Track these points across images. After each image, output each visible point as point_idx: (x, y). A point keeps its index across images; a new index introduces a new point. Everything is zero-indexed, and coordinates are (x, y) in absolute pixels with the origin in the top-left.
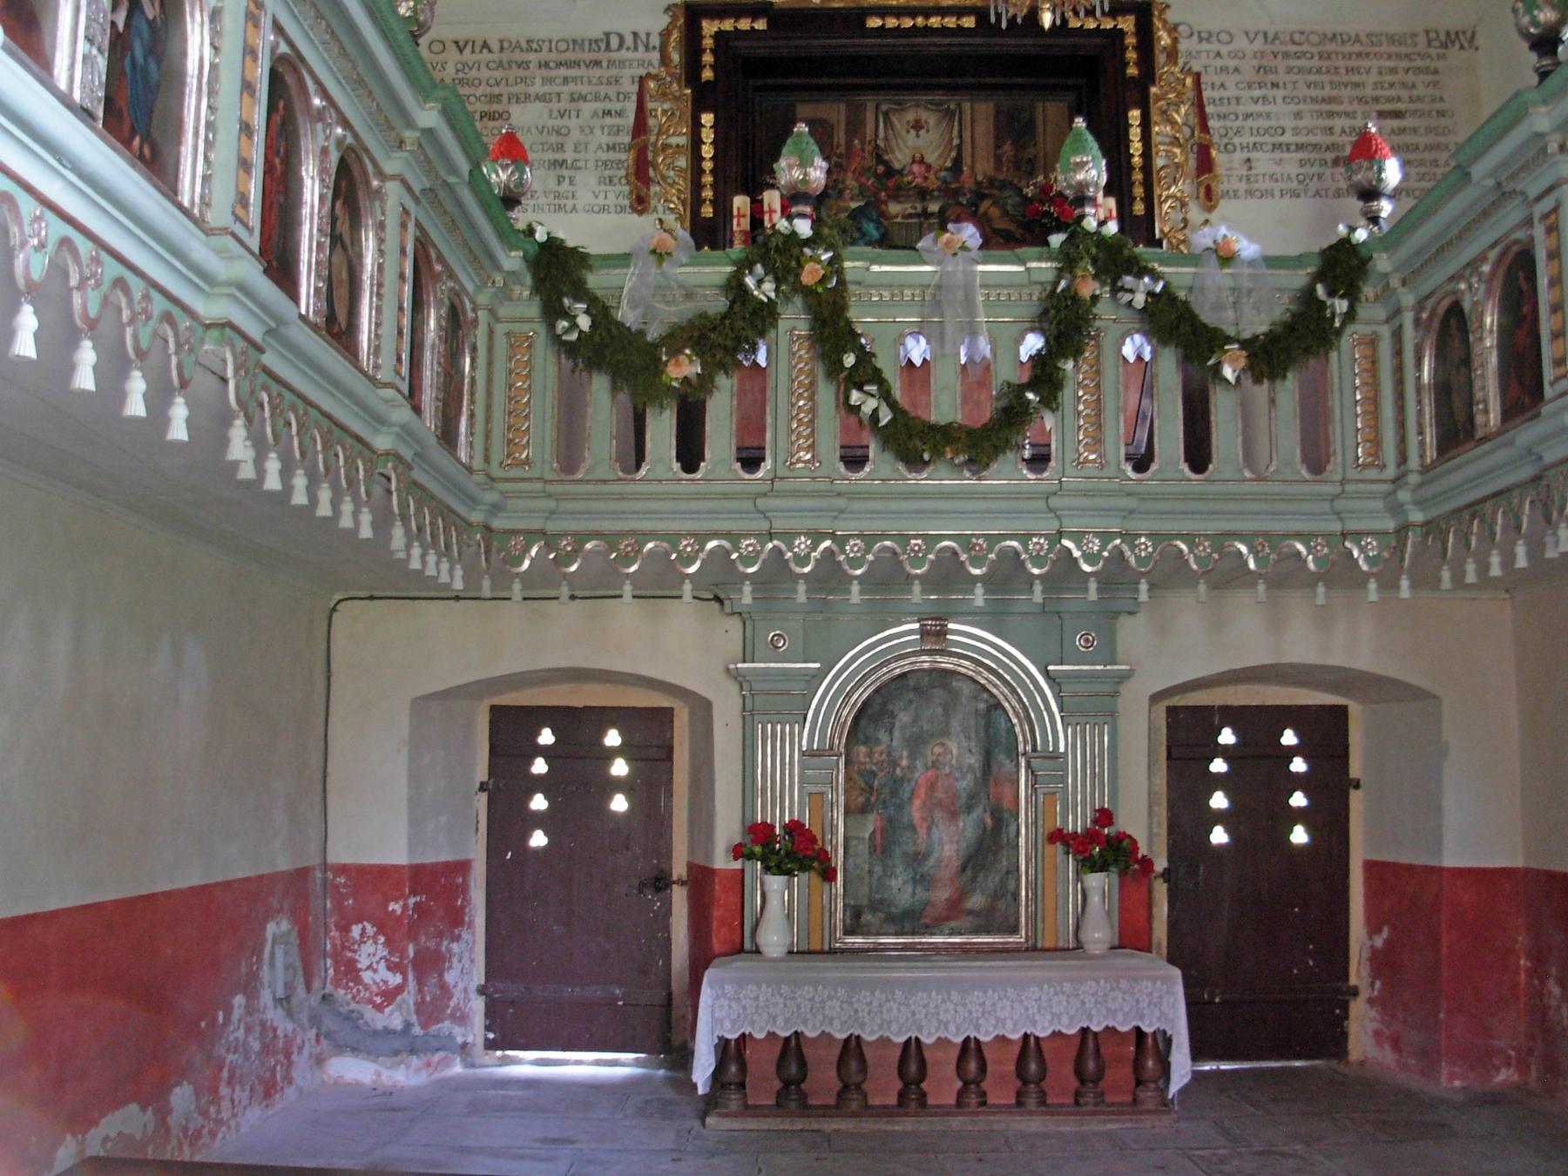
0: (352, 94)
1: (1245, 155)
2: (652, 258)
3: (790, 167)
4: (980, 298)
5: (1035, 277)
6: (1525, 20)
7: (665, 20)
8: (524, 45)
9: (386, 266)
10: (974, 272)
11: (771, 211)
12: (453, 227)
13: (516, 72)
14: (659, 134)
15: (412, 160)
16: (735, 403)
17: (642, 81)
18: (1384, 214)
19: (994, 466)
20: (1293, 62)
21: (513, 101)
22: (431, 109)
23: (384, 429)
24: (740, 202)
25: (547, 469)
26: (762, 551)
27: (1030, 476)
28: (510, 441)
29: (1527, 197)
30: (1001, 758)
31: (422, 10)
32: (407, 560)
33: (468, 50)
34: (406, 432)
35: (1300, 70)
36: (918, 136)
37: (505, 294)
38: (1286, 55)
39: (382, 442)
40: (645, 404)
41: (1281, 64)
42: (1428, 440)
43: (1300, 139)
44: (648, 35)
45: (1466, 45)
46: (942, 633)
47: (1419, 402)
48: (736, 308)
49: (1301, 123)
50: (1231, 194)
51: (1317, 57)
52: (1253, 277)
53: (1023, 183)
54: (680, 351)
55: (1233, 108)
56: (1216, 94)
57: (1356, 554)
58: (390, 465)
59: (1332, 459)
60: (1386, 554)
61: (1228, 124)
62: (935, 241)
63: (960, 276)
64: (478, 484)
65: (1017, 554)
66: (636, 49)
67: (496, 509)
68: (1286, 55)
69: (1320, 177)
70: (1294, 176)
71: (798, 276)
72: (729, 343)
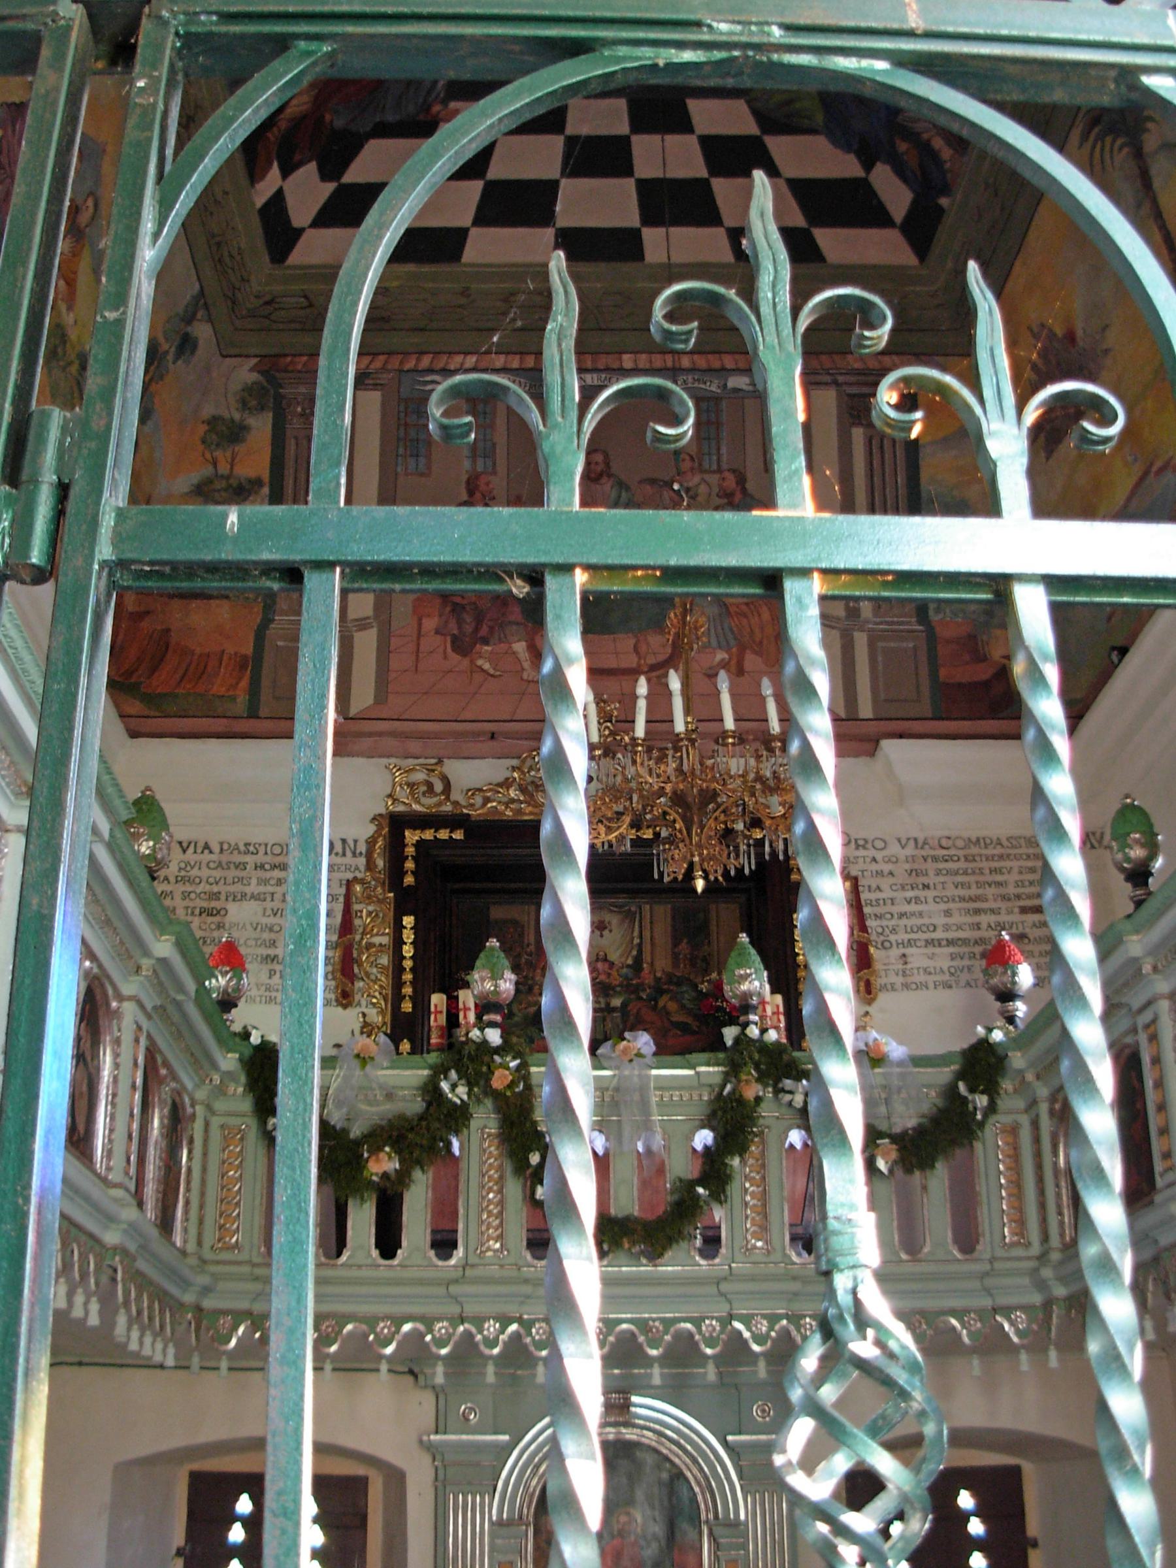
0: (100, 931)
1: (903, 951)
2: (356, 1063)
3: (483, 980)
4: (654, 1100)
5: (704, 1080)
6: (1119, 856)
7: (371, 829)
8: (242, 848)
9: (121, 1077)
10: (649, 1077)
11: (466, 1009)
12: (178, 1035)
13: (233, 873)
14: (364, 933)
15: (148, 985)
16: (430, 1194)
17: (349, 884)
18: (1020, 1014)
19: (669, 1254)
20: (942, 865)
21: (230, 899)
22: (167, 940)
23: (114, 1226)
24: (438, 1000)
25: (255, 1253)
26: (454, 1334)
27: (703, 1262)
28: (221, 1227)
29: (1130, 1010)
30: (684, 1526)
31: (160, 849)
32: (126, 1344)
33: (191, 849)
34: (133, 1229)
35: (949, 872)
36: (602, 936)
37: (221, 1091)
38: (935, 859)
39: (111, 1237)
40: (347, 1197)
41: (930, 866)
42: (1066, 1220)
43: (951, 935)
44: (356, 841)
45: (1096, 844)
46: (626, 1406)
47: (1057, 1186)
48: (432, 1110)
49: (950, 921)
50: (889, 987)
51: (963, 859)
52: (902, 1076)
53: (698, 980)
54: (381, 1149)
55: (889, 908)
56: (873, 896)
57: (1007, 1326)
58: (117, 1258)
59: (981, 1239)
60: (1035, 1327)
61: (884, 923)
62: (614, 1045)
63: (636, 1080)
64: (191, 1267)
65: (691, 1336)
66: (344, 855)
67: (206, 1290)
68: (935, 859)
69: (969, 968)
70: (945, 969)
71: (488, 1080)
72: (425, 1142)
